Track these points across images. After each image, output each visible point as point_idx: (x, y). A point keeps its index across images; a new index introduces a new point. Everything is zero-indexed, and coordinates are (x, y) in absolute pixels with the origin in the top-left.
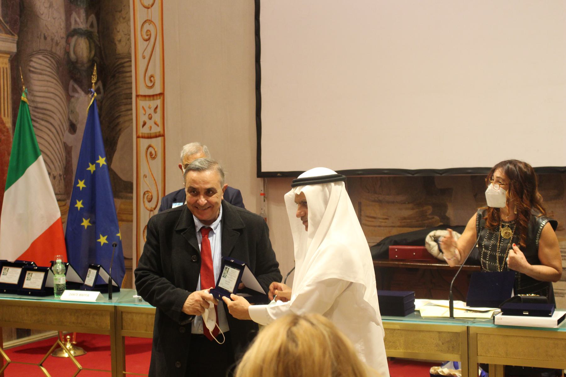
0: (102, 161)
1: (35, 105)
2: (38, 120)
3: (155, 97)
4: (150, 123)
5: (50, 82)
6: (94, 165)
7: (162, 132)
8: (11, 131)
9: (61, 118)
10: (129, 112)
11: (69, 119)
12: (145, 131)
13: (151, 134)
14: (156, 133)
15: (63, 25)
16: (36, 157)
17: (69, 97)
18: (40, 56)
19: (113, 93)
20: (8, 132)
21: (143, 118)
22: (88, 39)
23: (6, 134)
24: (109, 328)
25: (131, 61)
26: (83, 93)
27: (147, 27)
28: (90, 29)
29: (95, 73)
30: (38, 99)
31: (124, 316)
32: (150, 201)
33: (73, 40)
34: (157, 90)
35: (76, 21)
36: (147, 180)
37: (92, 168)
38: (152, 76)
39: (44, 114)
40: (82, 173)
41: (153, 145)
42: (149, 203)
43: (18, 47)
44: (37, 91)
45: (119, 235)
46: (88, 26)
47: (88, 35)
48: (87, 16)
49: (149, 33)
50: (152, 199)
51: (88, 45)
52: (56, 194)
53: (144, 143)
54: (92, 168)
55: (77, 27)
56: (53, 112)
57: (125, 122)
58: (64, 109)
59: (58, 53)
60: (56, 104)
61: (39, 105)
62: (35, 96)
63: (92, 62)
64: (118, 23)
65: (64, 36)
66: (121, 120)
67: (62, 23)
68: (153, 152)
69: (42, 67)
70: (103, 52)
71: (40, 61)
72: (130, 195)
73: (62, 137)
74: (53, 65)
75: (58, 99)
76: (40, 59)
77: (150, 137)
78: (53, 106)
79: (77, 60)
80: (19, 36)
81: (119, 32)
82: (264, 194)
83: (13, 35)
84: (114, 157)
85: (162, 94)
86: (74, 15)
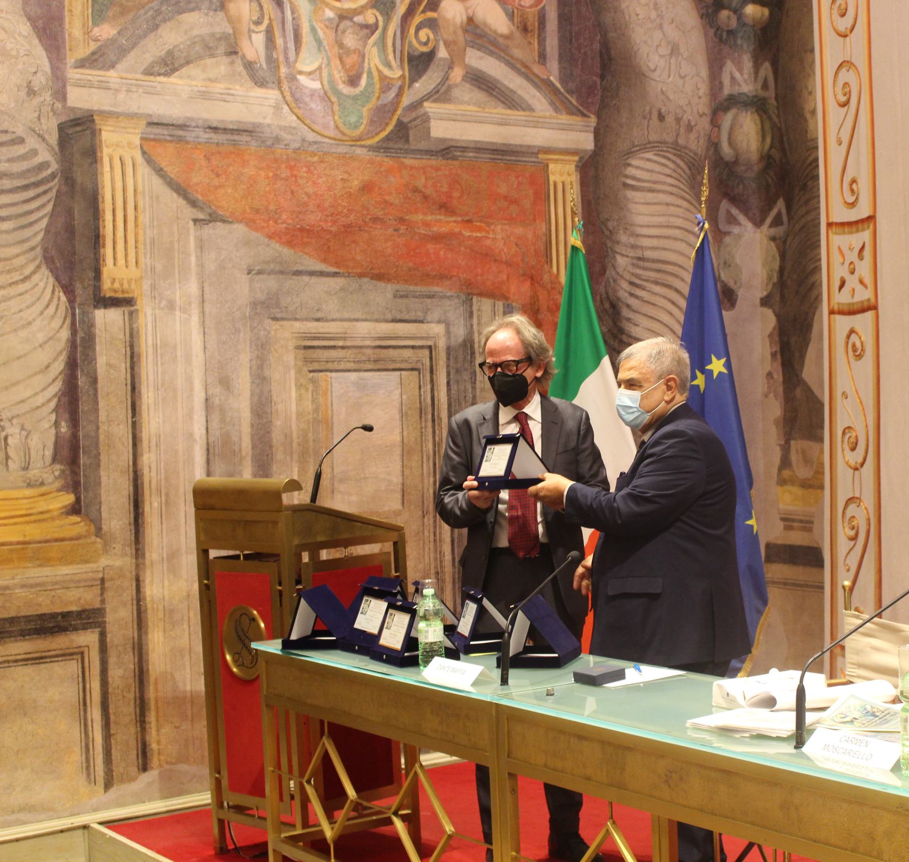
1: (639, 253)
2: (645, 284)
5: (673, 205)
12: (843, 298)
13: (853, 304)
14: (862, 302)
15: (704, 89)
18: (649, 155)
21: (840, 272)
22: (758, 114)
26: (749, 225)
27: (844, 76)
28: (761, 93)
30: (646, 242)
33: (727, 119)
34: (863, 211)
35: (733, 78)
41: (857, 329)
46: (759, 87)
47: (758, 105)
48: (757, 67)
49: (847, 90)
50: (856, 444)
51: (760, 126)
53: (843, 324)
55: (736, 90)
56: (680, 266)
59: (693, 146)
61: (649, 254)
64: (809, 75)
65: (707, 111)
67: (700, 85)
68: (858, 345)
69: (655, 177)
70: (785, 139)
71: (649, 165)
77: (851, 311)
80: (599, 117)
83: (584, 115)
84: (808, 354)
85: (871, 218)
86: (729, 67)
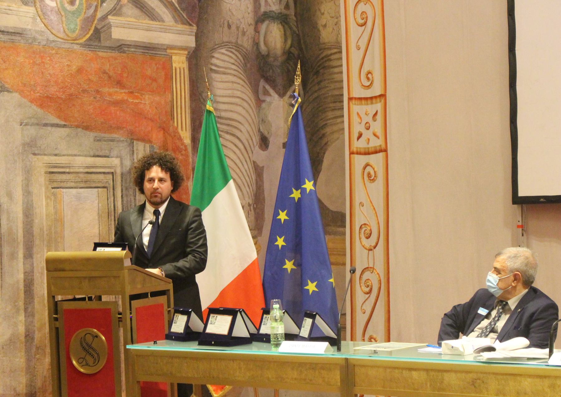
0: (309, 186)
3: (374, 101)
4: (367, 134)
5: (235, 83)
6: (299, 191)
7: (383, 147)
8: (190, 149)
9: (249, 129)
10: (339, 120)
11: (259, 130)
12: (360, 144)
13: (368, 148)
14: (375, 147)
15: (251, 8)
16: (226, 181)
17: (259, 102)
18: (223, 51)
19: (316, 95)
20: (186, 150)
21: (357, 128)
23: (184, 152)
24: (339, 384)
25: (340, 52)
26: (276, 96)
28: (285, 12)
29: (298, 73)
31: (357, 369)
32: (368, 238)
33: (263, 27)
34: (377, 90)
36: (364, 209)
37: (296, 195)
38: (369, 73)
39: (228, 125)
40: (282, 201)
41: (371, 163)
42: (366, 240)
43: (197, 41)
44: (220, 96)
45: (332, 280)
46: (283, 8)
47: (283, 19)
49: (364, 16)
50: (371, 234)
51: (283, 32)
52: (250, 230)
53: (360, 161)
54: (296, 195)
55: (268, 9)
57: (333, 133)
58: (253, 117)
59: (245, 45)
60: (243, 112)
61: (223, 114)
62: (218, 102)
63: (289, 56)
66: (328, 130)
70: (302, 41)
72: (341, 229)
73: (250, 155)
74: (238, 61)
75: (245, 105)
76: (223, 54)
78: (240, 114)
79: (269, 53)
80: (198, 27)
81: (323, 14)
82: (522, 226)
83: (190, 25)
85: (383, 96)
